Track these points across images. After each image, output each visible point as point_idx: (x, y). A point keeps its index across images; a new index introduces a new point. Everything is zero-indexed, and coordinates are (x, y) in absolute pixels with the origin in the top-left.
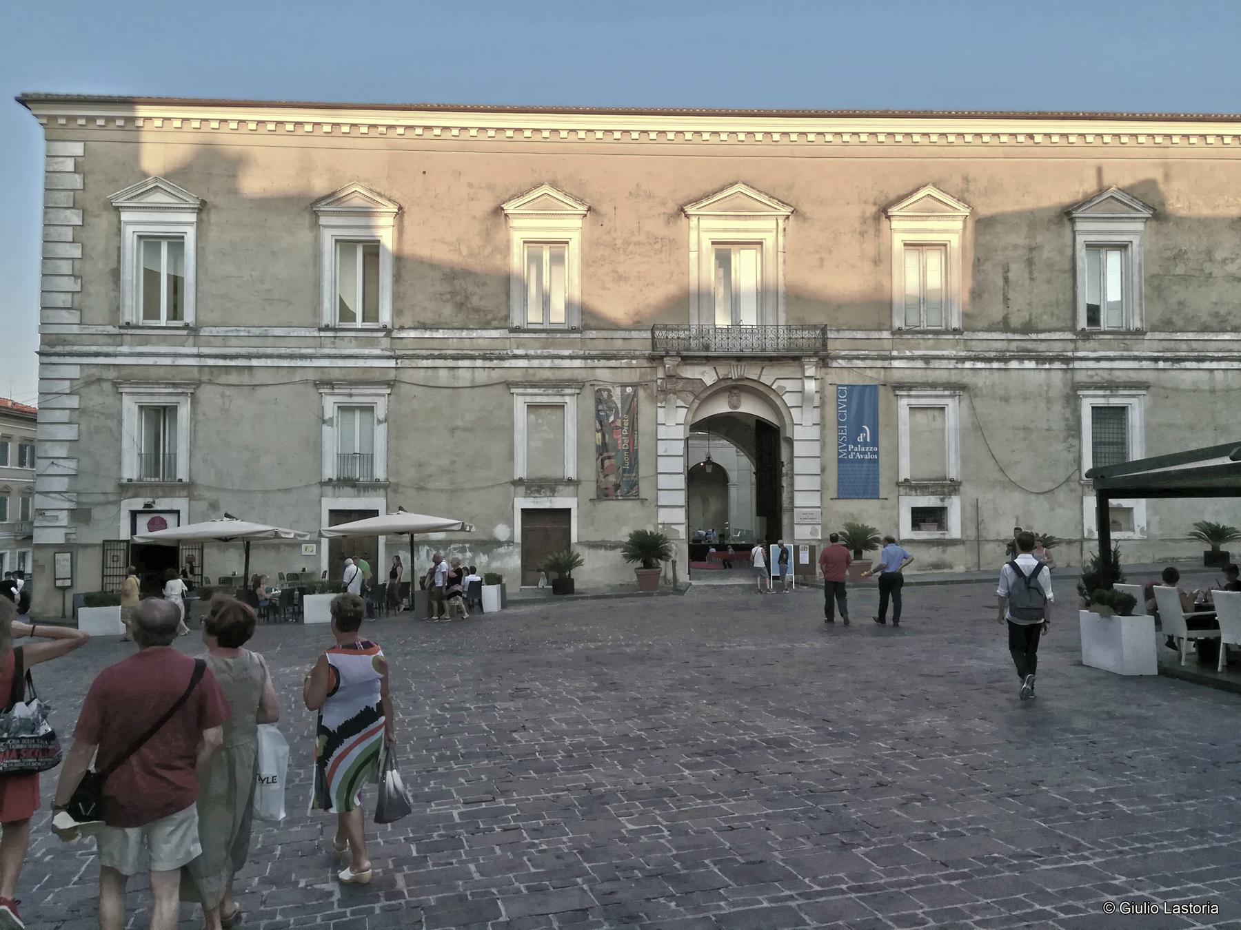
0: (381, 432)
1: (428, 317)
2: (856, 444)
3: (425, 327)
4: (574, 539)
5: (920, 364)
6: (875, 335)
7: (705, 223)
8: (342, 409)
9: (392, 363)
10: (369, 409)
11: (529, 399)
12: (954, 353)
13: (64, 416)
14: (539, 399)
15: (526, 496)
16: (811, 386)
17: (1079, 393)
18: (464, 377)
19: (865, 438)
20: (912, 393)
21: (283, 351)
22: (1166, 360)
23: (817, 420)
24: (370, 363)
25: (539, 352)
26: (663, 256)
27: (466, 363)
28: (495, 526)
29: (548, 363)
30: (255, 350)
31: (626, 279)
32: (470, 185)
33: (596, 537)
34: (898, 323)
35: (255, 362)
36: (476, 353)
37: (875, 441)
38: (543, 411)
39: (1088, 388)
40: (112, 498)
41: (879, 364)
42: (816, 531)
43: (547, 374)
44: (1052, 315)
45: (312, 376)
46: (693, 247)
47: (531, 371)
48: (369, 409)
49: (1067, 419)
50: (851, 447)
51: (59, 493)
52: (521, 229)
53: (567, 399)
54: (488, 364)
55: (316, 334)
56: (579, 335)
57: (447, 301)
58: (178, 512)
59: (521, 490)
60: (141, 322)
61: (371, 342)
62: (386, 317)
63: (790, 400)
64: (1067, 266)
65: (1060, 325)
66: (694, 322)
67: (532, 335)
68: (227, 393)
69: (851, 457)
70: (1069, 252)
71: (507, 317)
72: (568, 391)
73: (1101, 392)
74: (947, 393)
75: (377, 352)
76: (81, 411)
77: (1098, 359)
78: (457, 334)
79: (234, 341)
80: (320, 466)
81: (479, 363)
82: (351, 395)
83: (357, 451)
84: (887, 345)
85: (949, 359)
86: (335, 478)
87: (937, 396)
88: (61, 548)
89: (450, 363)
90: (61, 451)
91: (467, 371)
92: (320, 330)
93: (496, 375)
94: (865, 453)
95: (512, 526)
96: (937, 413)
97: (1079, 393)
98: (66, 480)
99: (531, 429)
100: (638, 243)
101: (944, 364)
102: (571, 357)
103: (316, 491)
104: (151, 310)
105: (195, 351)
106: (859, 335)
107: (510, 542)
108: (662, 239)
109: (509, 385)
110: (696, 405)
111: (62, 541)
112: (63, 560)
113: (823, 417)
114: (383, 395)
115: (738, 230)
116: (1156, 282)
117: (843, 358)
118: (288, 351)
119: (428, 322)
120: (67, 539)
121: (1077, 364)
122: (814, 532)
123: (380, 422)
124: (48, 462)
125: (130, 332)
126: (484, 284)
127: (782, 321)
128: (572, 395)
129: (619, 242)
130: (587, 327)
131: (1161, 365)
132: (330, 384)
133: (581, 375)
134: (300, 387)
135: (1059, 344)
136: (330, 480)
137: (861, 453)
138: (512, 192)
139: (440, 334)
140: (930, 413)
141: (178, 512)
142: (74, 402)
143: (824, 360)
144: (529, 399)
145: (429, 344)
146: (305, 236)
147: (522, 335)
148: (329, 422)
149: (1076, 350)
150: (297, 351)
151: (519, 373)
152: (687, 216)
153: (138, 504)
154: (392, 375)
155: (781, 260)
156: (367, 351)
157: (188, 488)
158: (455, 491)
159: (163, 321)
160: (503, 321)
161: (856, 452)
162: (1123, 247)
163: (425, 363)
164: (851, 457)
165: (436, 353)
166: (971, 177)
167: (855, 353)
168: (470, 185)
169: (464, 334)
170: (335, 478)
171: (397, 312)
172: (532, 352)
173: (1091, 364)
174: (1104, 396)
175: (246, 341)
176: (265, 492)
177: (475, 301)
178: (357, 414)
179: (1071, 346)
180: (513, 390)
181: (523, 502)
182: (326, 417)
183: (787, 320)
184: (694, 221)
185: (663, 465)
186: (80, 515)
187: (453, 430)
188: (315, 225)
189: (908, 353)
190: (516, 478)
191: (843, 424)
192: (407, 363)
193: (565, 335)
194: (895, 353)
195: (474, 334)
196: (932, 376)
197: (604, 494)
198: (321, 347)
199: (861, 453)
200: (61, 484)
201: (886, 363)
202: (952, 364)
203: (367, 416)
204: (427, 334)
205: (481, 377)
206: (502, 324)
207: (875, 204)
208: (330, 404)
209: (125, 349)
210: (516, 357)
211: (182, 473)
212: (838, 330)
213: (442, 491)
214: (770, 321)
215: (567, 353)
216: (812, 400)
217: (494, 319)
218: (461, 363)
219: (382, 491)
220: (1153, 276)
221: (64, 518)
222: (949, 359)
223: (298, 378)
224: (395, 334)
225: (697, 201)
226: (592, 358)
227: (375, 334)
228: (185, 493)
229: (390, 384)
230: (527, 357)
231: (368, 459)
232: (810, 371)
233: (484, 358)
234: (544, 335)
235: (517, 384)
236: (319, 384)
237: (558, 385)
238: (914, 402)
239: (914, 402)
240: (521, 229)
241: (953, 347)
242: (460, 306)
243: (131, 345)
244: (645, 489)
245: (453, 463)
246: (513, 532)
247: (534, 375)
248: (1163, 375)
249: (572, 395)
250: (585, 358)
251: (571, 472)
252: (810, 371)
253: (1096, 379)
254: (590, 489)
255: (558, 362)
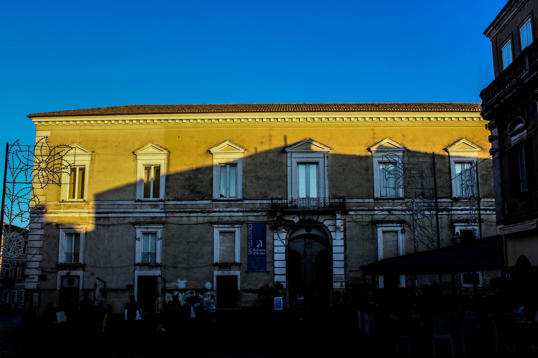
0: (159, 243)
1: (179, 195)
2: (256, 248)
3: (177, 199)
4: (239, 289)
5: (386, 213)
6: (367, 200)
7: (294, 155)
8: (144, 234)
9: (164, 215)
10: (155, 234)
11: (220, 229)
12: (401, 208)
13: (38, 237)
14: (224, 229)
15: (219, 270)
16: (339, 223)
17: (455, 224)
18: (194, 220)
19: (260, 246)
20: (384, 225)
21: (121, 210)
22: (490, 210)
23: (342, 237)
24: (138, 215)
25: (224, 209)
26: (276, 169)
27: (195, 214)
28: (205, 283)
29: (228, 214)
30: (110, 210)
31: (261, 179)
32: (197, 142)
33: (248, 288)
34: (377, 195)
35: (110, 215)
36: (199, 210)
37: (264, 247)
38: (226, 234)
39: (458, 222)
40: (54, 270)
41: (369, 213)
42: (343, 285)
43: (227, 219)
44: (442, 191)
45: (132, 220)
46: (289, 164)
47: (221, 218)
48: (155, 234)
49: (449, 236)
50: (254, 249)
51: (36, 268)
52: (217, 159)
53: (236, 229)
54: (203, 215)
55: (134, 203)
56: (241, 202)
57: (187, 189)
58: (79, 276)
59: (217, 268)
60: (68, 200)
61: (156, 206)
62: (162, 196)
63: (331, 229)
64: (447, 171)
65: (446, 196)
66: (289, 197)
67: (221, 203)
68: (99, 227)
69: (254, 254)
70: (447, 165)
71: (211, 195)
72: (236, 226)
73: (463, 224)
74: (398, 225)
75: (158, 210)
76: (44, 235)
77: (462, 210)
78: (191, 202)
79: (102, 207)
80: (135, 258)
81: (200, 214)
82: (147, 228)
83: (150, 251)
84: (372, 204)
85: (399, 210)
86: (140, 262)
87: (394, 226)
88: (34, 290)
89: (188, 215)
90: (35, 251)
91: (194, 218)
92: (136, 201)
93: (206, 219)
94: (260, 252)
95: (212, 282)
96: (395, 234)
97: (455, 224)
98: (38, 263)
99: (222, 242)
100: (266, 163)
101: (397, 213)
102: (238, 212)
103: (132, 268)
104: (147, 195)
105: (87, 211)
106: (360, 200)
107: (212, 290)
108: (276, 161)
109: (211, 223)
110: (291, 231)
111: (35, 287)
112: (36, 295)
113: (345, 236)
114: (160, 228)
115: (308, 158)
116: (485, 177)
117: (353, 210)
118: (123, 210)
119: (179, 198)
120: (37, 287)
121: (453, 212)
122: (342, 285)
123: (159, 239)
124: (31, 256)
125: (64, 203)
126: (202, 182)
127: (327, 196)
128: (238, 227)
129: (258, 163)
130: (244, 199)
131: (488, 212)
132: (139, 224)
133: (242, 219)
134: (128, 226)
135: (446, 204)
136: (139, 263)
137: (258, 252)
138: (214, 144)
139: (184, 202)
140: (392, 234)
141: (79, 276)
142: (42, 232)
143: (345, 212)
144: (220, 229)
145: (179, 207)
146: (132, 163)
147: (217, 203)
148: (139, 239)
149: (452, 206)
150: (126, 210)
151: (216, 218)
152: (287, 153)
153: (64, 273)
154: (164, 219)
155: (326, 170)
156: (154, 210)
157: (83, 267)
158: (189, 269)
159: (151, 198)
160: (210, 196)
161: (256, 252)
162: (317, 163)
163: (178, 215)
164: (254, 254)
165: (182, 210)
166: (405, 135)
167: (358, 208)
168: (197, 142)
169: (194, 202)
170: (140, 262)
171: (167, 193)
172: (221, 210)
173: (459, 212)
174: (465, 226)
175: (107, 207)
176: (112, 268)
177: (199, 189)
178: (150, 236)
179: (450, 204)
180: (213, 226)
181: (216, 273)
182: (137, 237)
183: (329, 195)
184: (289, 155)
185: (277, 257)
186: (42, 278)
187: (189, 242)
188: (136, 159)
189: (381, 208)
190: (214, 262)
191: (250, 240)
192: (170, 215)
193: (235, 203)
194: (375, 208)
195: (198, 202)
196: (392, 218)
197: (250, 269)
198: (136, 208)
199: (258, 252)
200: (36, 265)
201: (372, 213)
202: (400, 213)
203: (154, 236)
204: (179, 203)
205: (201, 220)
206: (210, 198)
207: (366, 146)
208: (139, 232)
209: (61, 211)
210: (215, 212)
211: (81, 261)
212: (351, 199)
213: (184, 268)
214: (322, 196)
215: (236, 210)
216: (340, 228)
217: (206, 196)
218: (192, 215)
219: (159, 268)
220: (483, 175)
221: (36, 279)
222: (399, 210)
223: (126, 221)
224: (166, 203)
225: (451, 145)
226: (247, 212)
227: (158, 203)
228: (82, 269)
229: (163, 223)
230: (219, 211)
231: (154, 255)
232: (339, 216)
233: (202, 212)
234: (226, 202)
235: (215, 223)
236: (134, 224)
237: (233, 223)
238: (384, 229)
239: (384, 229)
240: (217, 159)
241: (401, 205)
242: (192, 191)
243: (64, 209)
244: (269, 268)
245: (189, 256)
246: (213, 285)
247: (222, 219)
248: (489, 217)
249: (238, 227)
250: (243, 212)
251: (238, 260)
252: (339, 216)
253: (461, 218)
254: (245, 267)
255: (232, 214)
